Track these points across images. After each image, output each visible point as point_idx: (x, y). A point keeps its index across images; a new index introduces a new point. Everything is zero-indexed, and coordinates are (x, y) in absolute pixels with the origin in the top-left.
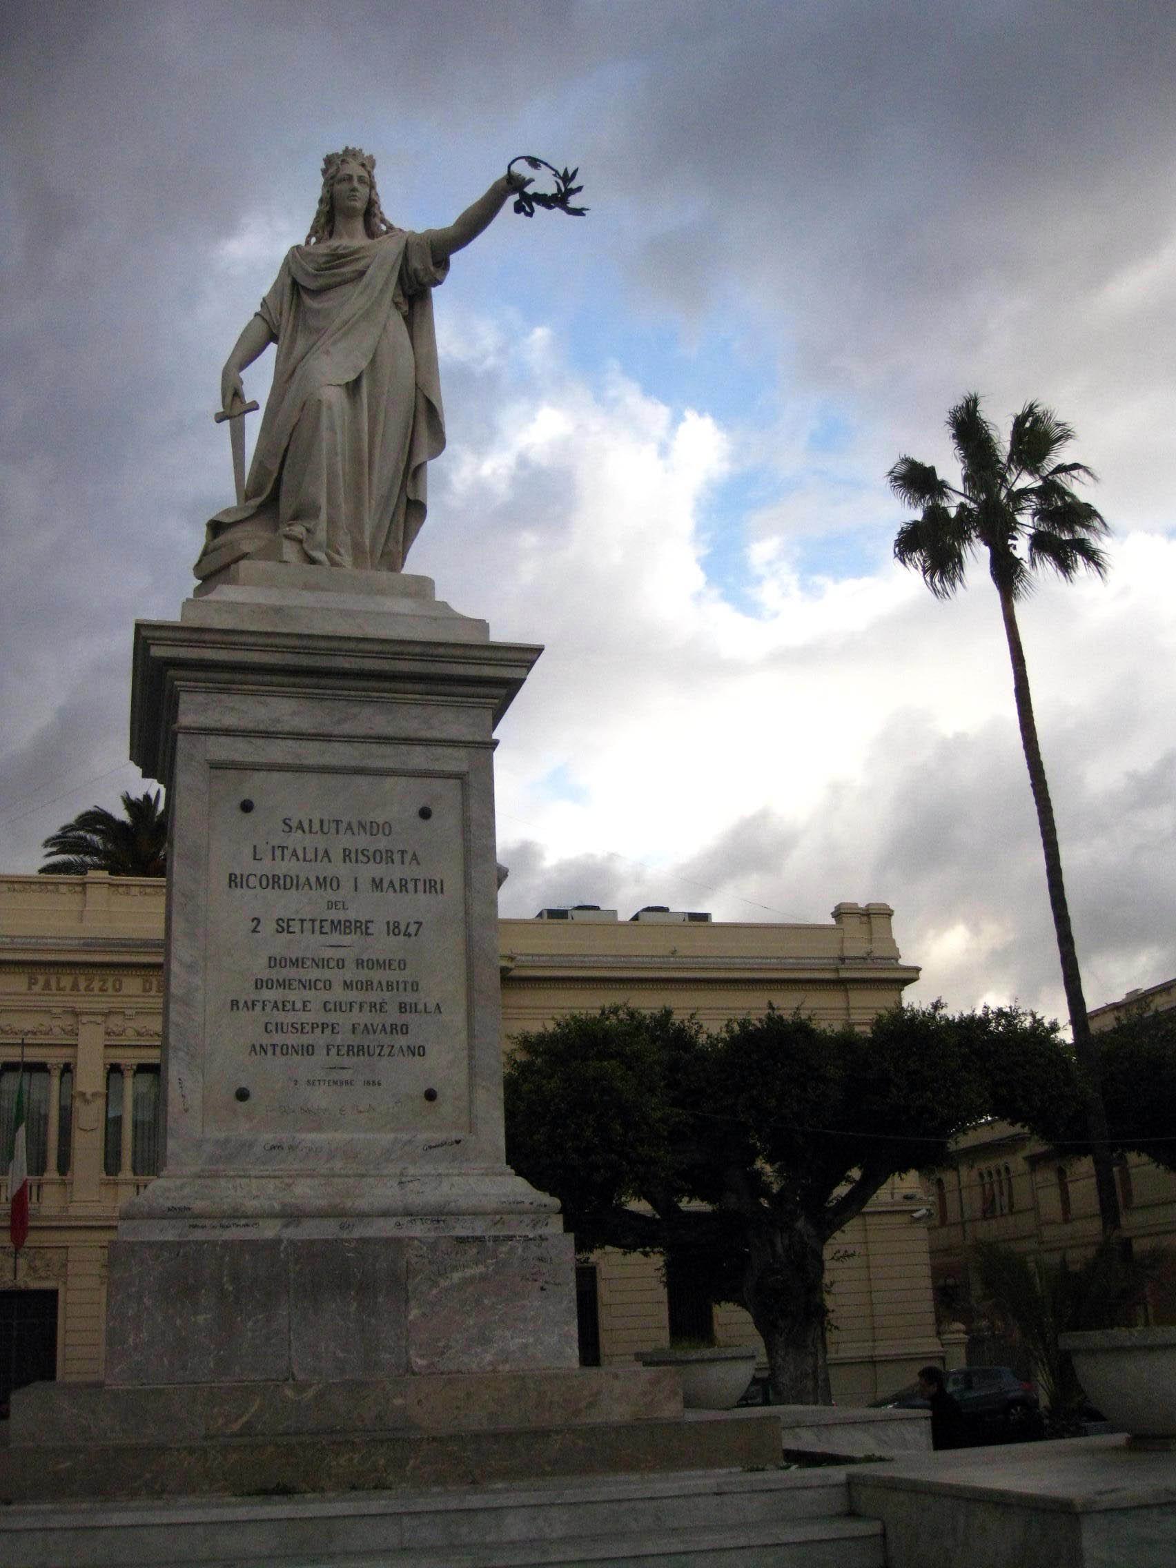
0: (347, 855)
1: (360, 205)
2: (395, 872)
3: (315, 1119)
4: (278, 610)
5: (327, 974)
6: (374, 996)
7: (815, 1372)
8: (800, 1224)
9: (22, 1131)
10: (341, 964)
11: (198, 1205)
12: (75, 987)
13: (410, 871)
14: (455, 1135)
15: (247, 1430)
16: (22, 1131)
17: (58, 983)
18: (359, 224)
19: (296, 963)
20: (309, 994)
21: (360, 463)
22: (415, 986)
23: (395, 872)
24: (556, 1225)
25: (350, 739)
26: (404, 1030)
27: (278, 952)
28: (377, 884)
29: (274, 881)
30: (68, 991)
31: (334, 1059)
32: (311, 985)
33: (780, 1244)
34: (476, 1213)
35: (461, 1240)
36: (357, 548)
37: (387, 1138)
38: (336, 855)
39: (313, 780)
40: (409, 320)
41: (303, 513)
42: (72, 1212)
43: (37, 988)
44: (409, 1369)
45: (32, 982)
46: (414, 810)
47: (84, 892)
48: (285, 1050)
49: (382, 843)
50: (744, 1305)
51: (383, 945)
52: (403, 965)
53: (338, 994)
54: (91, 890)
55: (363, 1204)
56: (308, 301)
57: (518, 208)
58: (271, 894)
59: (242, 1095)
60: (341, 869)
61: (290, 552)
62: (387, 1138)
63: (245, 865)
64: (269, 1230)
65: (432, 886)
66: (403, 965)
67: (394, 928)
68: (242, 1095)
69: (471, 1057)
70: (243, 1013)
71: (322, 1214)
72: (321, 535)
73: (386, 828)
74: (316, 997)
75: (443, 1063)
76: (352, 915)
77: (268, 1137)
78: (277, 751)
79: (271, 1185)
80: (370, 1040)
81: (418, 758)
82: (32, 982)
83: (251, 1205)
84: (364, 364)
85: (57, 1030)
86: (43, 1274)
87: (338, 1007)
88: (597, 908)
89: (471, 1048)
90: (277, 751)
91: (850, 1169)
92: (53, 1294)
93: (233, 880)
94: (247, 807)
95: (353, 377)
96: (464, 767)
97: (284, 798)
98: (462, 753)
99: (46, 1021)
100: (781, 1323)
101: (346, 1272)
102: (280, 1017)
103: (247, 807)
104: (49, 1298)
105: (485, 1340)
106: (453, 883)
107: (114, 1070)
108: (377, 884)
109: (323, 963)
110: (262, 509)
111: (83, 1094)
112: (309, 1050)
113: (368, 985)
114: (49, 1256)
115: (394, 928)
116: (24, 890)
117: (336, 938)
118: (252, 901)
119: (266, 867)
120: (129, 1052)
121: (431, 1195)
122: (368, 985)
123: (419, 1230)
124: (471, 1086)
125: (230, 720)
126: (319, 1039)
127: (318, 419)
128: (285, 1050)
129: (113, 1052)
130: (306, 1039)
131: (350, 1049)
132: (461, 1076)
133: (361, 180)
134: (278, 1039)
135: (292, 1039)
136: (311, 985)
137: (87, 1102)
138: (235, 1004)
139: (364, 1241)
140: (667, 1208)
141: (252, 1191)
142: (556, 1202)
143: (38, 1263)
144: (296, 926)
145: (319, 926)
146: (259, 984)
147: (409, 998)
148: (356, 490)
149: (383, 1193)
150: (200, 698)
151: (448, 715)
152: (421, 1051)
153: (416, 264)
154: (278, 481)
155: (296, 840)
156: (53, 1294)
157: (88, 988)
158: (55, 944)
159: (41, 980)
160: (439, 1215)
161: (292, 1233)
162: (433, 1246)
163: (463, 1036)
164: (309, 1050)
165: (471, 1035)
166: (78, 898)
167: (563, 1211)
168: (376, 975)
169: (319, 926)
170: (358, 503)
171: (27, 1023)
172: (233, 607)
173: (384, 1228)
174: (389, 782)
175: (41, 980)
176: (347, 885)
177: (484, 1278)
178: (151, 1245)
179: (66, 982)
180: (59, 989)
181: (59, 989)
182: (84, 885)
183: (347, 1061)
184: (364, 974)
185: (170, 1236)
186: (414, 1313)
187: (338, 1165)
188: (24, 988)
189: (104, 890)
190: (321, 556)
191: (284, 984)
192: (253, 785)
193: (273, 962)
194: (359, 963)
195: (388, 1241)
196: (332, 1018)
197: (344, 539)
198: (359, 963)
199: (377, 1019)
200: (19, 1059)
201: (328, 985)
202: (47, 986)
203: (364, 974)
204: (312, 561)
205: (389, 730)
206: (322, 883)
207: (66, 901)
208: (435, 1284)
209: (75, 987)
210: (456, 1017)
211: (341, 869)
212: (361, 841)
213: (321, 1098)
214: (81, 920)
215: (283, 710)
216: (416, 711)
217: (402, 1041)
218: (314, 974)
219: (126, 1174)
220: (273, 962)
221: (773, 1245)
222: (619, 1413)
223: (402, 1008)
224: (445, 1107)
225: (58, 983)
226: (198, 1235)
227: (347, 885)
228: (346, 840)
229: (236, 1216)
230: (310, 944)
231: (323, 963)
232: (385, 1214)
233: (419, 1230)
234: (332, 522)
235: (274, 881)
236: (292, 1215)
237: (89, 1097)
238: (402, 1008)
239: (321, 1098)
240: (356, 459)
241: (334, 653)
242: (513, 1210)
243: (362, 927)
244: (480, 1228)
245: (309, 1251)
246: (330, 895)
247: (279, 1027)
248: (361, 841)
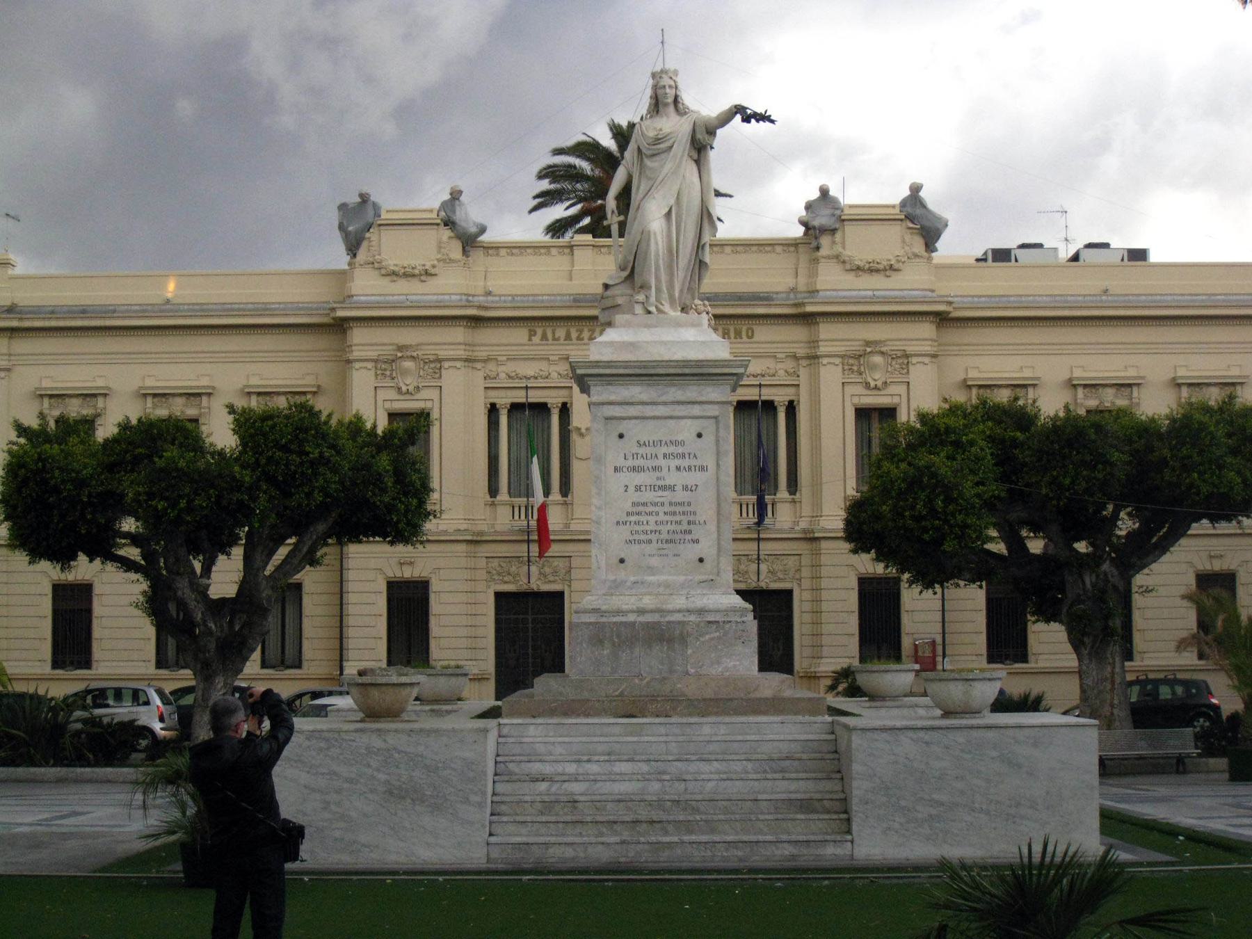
0: (665, 456)
1: (670, 100)
2: (685, 463)
3: (651, 570)
4: (632, 344)
5: (657, 509)
6: (678, 518)
7: (1113, 677)
8: (1106, 566)
9: (535, 459)
10: (663, 504)
11: (604, 608)
12: (568, 337)
13: (693, 462)
14: (711, 577)
15: (621, 694)
16: (535, 459)
17: (554, 333)
18: (672, 108)
19: (645, 504)
20: (650, 518)
21: (672, 254)
22: (695, 513)
23: (685, 463)
24: (751, 616)
25: (665, 403)
26: (690, 532)
27: (635, 500)
28: (678, 469)
29: (634, 469)
30: (562, 341)
31: (660, 545)
32: (650, 514)
33: (1088, 580)
34: (718, 611)
35: (709, 622)
36: (671, 297)
37: (682, 578)
38: (661, 456)
39: (652, 423)
40: (698, 162)
41: (644, 287)
42: (573, 527)
43: (536, 339)
44: (687, 673)
45: (532, 333)
46: (694, 435)
47: (572, 251)
48: (639, 542)
49: (680, 450)
50: (1061, 622)
51: (680, 496)
52: (689, 504)
53: (662, 517)
54: (577, 252)
55: (670, 607)
56: (648, 162)
57: (743, 120)
58: (633, 475)
59: (622, 561)
60: (661, 462)
61: (639, 309)
62: (682, 578)
63: (621, 462)
64: (631, 618)
65: (703, 469)
66: (689, 504)
67: (685, 488)
68: (622, 561)
69: (719, 544)
70: (622, 527)
71: (652, 611)
72: (653, 299)
73: (682, 443)
74: (652, 519)
75: (706, 547)
76: (668, 482)
77: (632, 579)
78: (632, 411)
79: (633, 599)
80: (677, 537)
81: (696, 410)
82: (532, 333)
83: (625, 607)
84: (672, 202)
85: (554, 375)
86: (552, 578)
87: (662, 523)
88: (1040, 246)
89: (719, 539)
90: (632, 411)
91: (1078, 540)
92: (560, 595)
93: (616, 469)
94: (621, 436)
95: (667, 210)
96: (717, 413)
97: (636, 431)
98: (716, 407)
99: (543, 365)
100: (1086, 639)
101: (662, 634)
102: (637, 528)
103: (621, 436)
104: (556, 599)
105: (719, 663)
106: (711, 464)
107: (493, 410)
108: (678, 469)
109: (656, 504)
110: (627, 278)
111: (578, 429)
112: (650, 542)
113: (674, 513)
114: (556, 564)
115: (685, 488)
116: (521, 254)
117: (660, 493)
118: (625, 477)
119: (630, 463)
120: (502, 393)
121: (699, 602)
122: (674, 513)
123: (692, 618)
124: (718, 555)
125: (613, 398)
126: (653, 537)
127: (649, 240)
128: (639, 542)
129: (492, 393)
130: (649, 537)
131: (667, 541)
132: (714, 551)
133: (670, 87)
134: (636, 537)
135: (643, 537)
136: (650, 514)
137: (582, 435)
138: (618, 523)
139: (669, 622)
140: (1017, 545)
141: (626, 601)
142: (751, 607)
143: (547, 570)
144: (643, 488)
145: (653, 488)
146: (628, 514)
147: (691, 518)
148: (671, 275)
149: (679, 602)
150: (599, 388)
151: (709, 389)
152: (697, 541)
153: (699, 136)
154: (633, 267)
155: (642, 451)
156: (560, 595)
157: (579, 338)
158: (548, 301)
159: (539, 332)
160: (701, 611)
161: (642, 619)
162: (698, 625)
163: (715, 535)
164: (650, 542)
165: (719, 535)
166: (566, 259)
167: (754, 611)
168: (678, 509)
169: (653, 488)
170: (671, 275)
171: (529, 369)
172: (611, 344)
173: (677, 617)
174: (683, 422)
175: (539, 332)
176: (665, 470)
177: (719, 638)
178: (585, 623)
179: (561, 333)
180: (554, 339)
181: (554, 339)
182: (571, 247)
183: (665, 546)
184: (673, 509)
185: (592, 620)
186: (690, 652)
187: (661, 590)
188: (525, 339)
189: (589, 251)
190: (653, 309)
191: (638, 514)
192: (622, 427)
193: (634, 504)
194: (671, 504)
195: (679, 622)
196: (658, 528)
197: (665, 295)
198: (671, 504)
199: (679, 528)
200: (523, 400)
201: (657, 514)
202: (544, 337)
203: (673, 509)
204: (649, 312)
205: (683, 398)
206: (655, 469)
207: (558, 262)
208: (697, 639)
209: (568, 337)
210: (712, 527)
211: (661, 462)
212: (672, 449)
213: (655, 562)
214: (571, 279)
215: (635, 391)
216: (695, 388)
217: (688, 537)
218: (651, 509)
219: (503, 495)
220: (634, 504)
221: (1083, 583)
222: (768, 693)
223: (689, 523)
224: (708, 565)
225: (554, 333)
226: (604, 620)
227: (665, 470)
228: (664, 450)
229: (619, 612)
230: (649, 496)
231: (656, 504)
232: (679, 611)
233: (692, 618)
234: (658, 290)
235: (634, 469)
236: (641, 612)
237: (583, 431)
238: (689, 523)
239: (655, 562)
240: (670, 251)
241: (653, 367)
242: (734, 610)
243: (672, 488)
244: (718, 618)
245: (647, 625)
246: (658, 474)
247: (637, 532)
248: (672, 449)
